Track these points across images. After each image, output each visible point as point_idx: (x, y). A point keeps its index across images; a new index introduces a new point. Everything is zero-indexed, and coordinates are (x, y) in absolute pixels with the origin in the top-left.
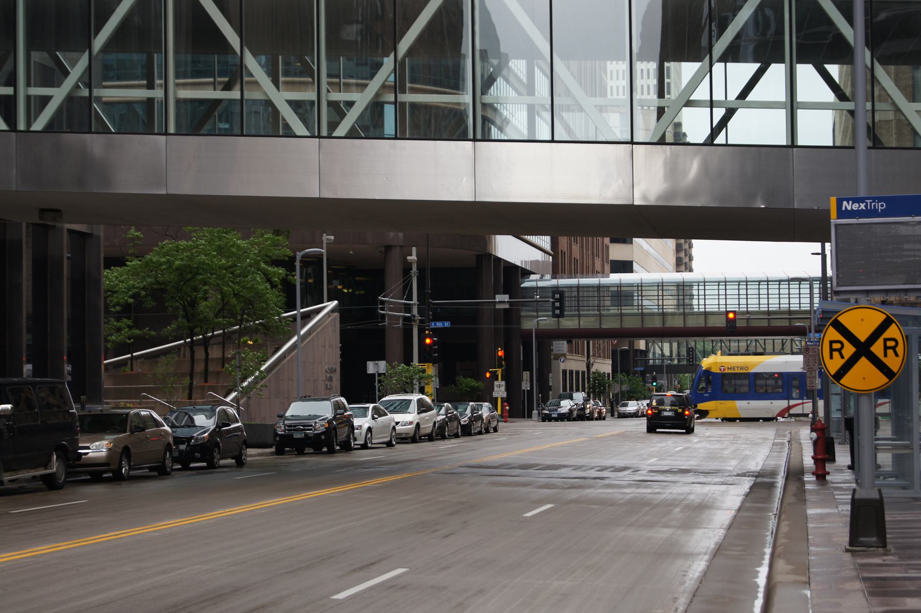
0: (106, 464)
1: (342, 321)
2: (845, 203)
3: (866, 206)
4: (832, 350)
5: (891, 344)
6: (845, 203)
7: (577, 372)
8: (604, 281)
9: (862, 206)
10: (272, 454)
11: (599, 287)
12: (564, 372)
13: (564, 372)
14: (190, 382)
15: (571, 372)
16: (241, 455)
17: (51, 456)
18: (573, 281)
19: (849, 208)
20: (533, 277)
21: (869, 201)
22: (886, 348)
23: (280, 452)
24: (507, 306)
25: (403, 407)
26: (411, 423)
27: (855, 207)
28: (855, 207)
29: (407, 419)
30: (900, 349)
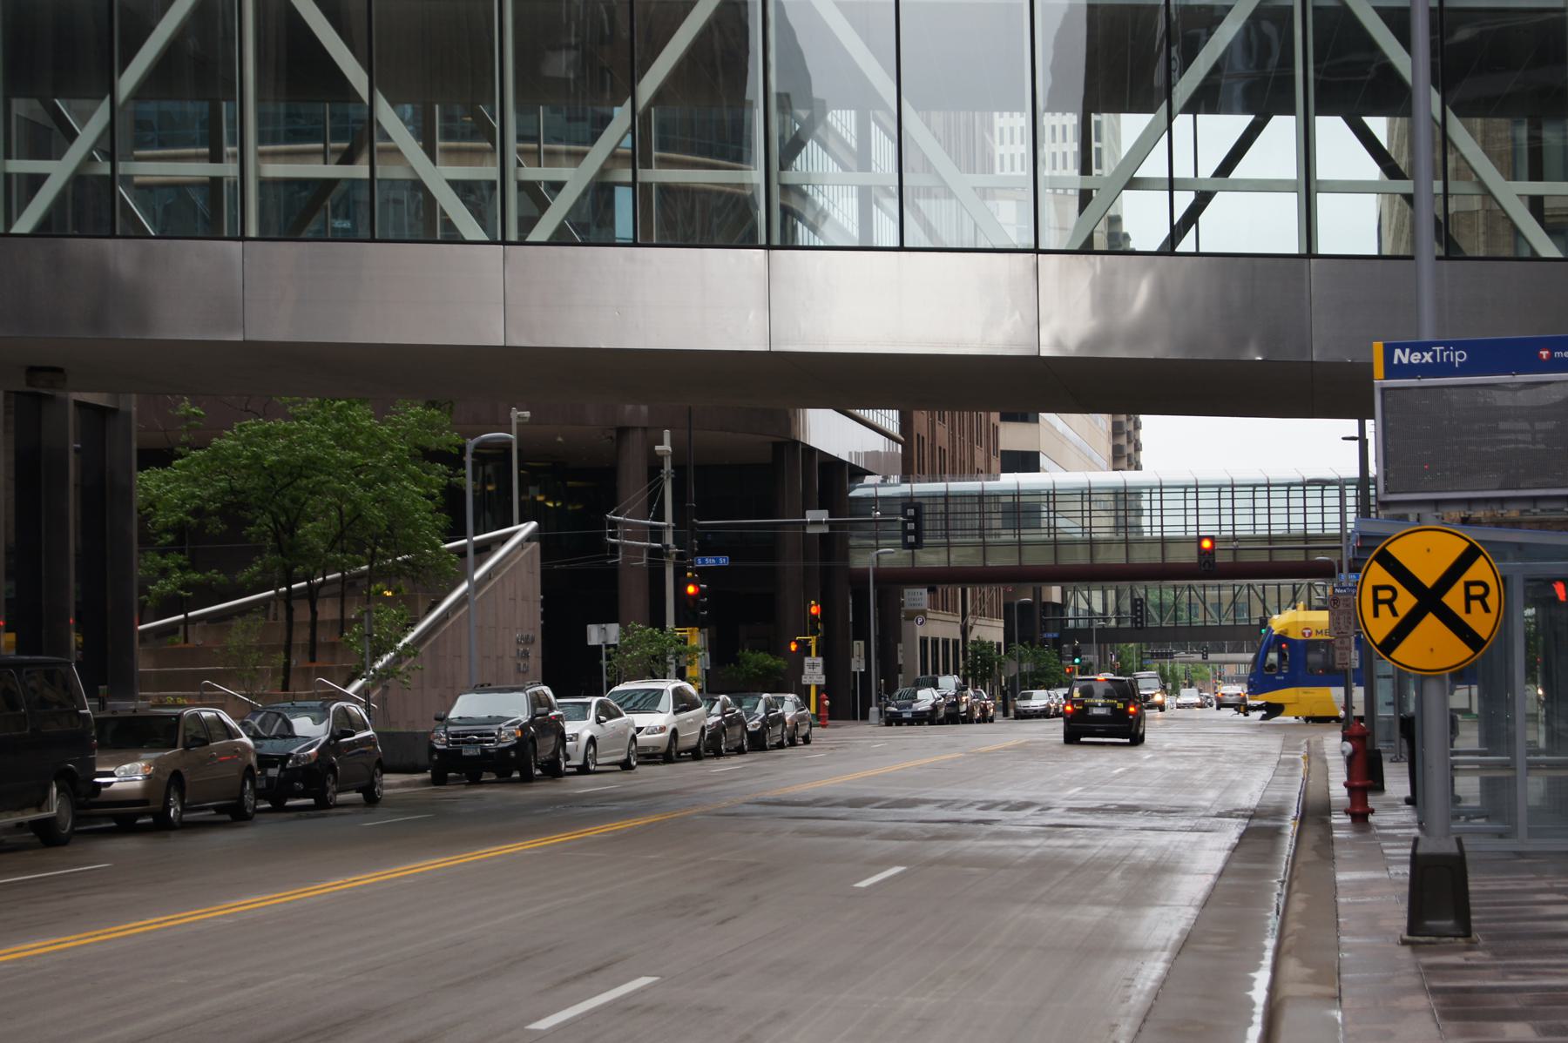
0: (143, 802)
1: (546, 555)
2: (1398, 352)
3: (1434, 357)
4: (1377, 602)
5: (1476, 591)
6: (1398, 352)
7: (946, 642)
8: (991, 486)
9: (1428, 357)
10: (425, 783)
11: (981, 497)
12: (924, 641)
13: (924, 641)
14: (286, 660)
15: (935, 641)
16: (372, 785)
17: (47, 789)
18: (938, 487)
19: (1405, 361)
20: (869, 480)
21: (1438, 349)
22: (1469, 598)
23: (439, 780)
24: (826, 530)
25: (649, 702)
26: (663, 729)
27: (1416, 358)
28: (1416, 358)
29: (656, 723)
30: (1492, 600)
